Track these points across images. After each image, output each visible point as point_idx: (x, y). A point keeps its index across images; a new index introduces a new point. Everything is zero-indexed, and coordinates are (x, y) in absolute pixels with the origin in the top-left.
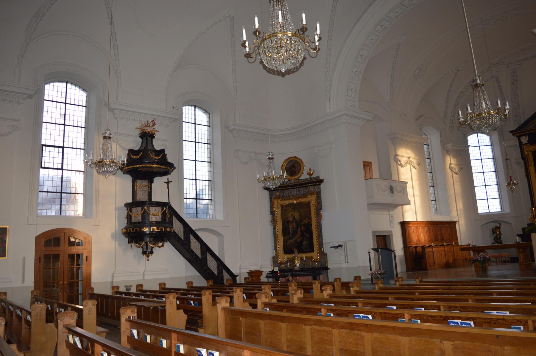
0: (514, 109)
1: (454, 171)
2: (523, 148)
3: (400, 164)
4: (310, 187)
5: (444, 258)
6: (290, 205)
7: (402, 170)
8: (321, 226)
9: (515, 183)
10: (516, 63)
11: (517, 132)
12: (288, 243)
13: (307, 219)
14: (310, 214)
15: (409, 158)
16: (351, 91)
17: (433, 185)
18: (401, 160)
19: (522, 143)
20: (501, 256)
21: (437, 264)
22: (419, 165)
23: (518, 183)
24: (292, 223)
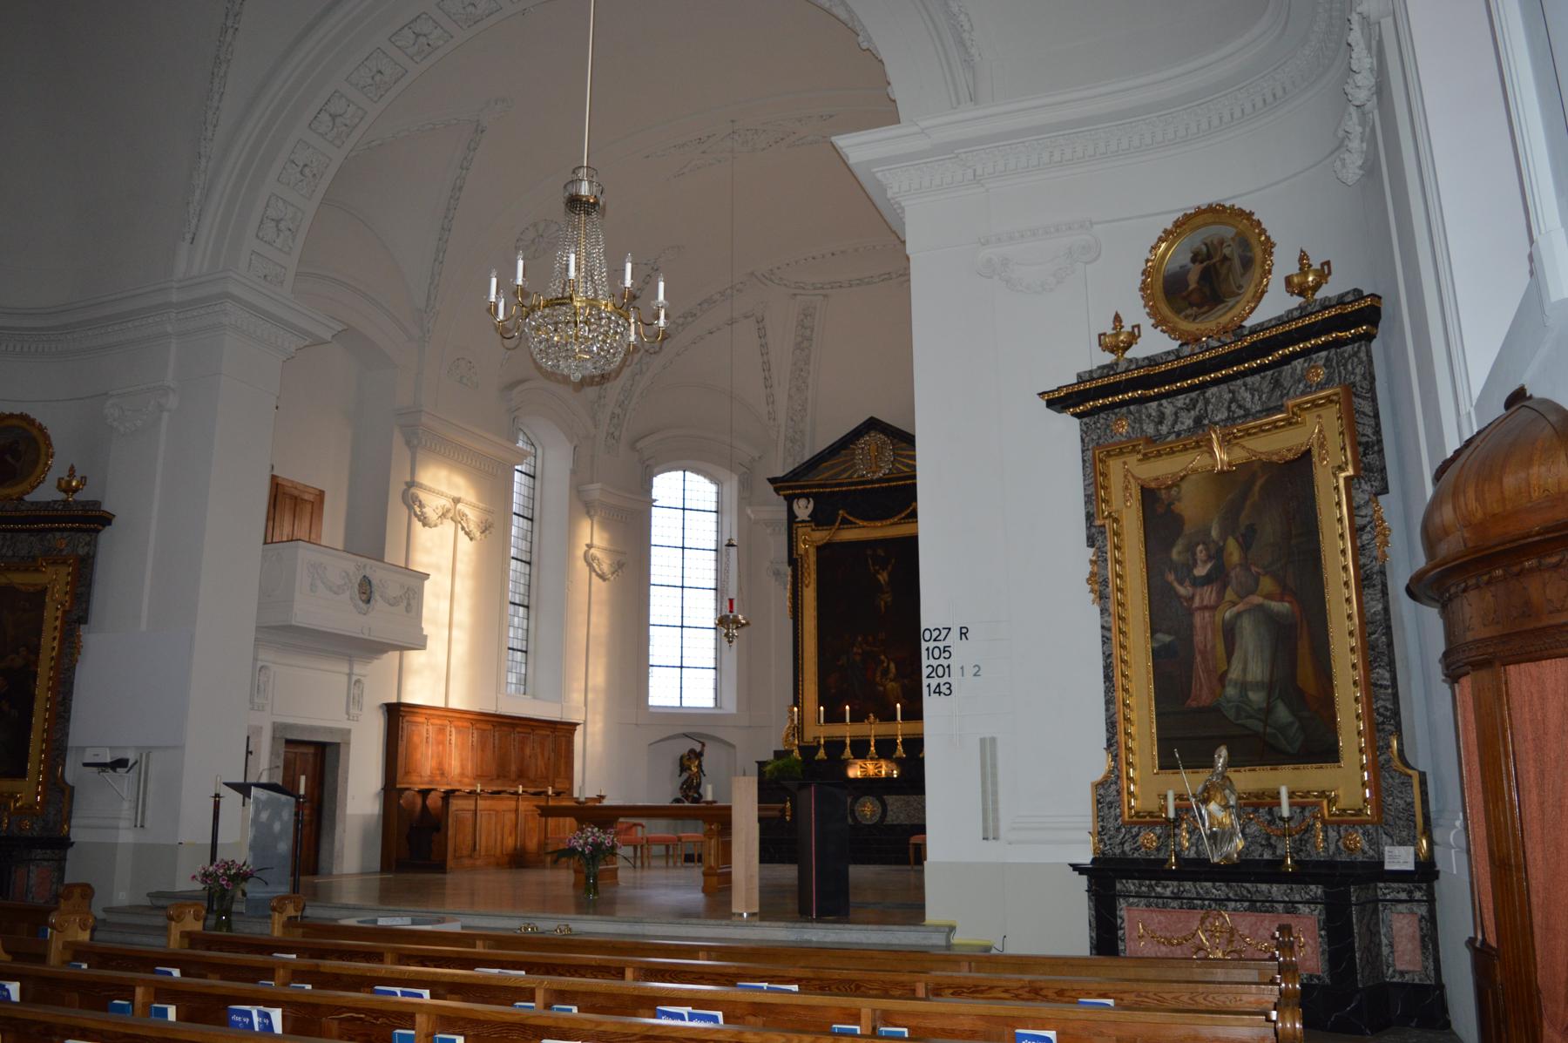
0: (792, 420)
1: (596, 567)
2: (796, 533)
3: (419, 513)
4: (58, 535)
5: (511, 835)
7: (422, 534)
8: (72, 684)
9: (739, 622)
10: (815, 289)
11: (787, 484)
14: (39, 632)
15: (457, 501)
16: (277, 226)
17: (526, 604)
18: (423, 502)
19: (797, 517)
20: (680, 839)
21: (483, 853)
22: (486, 529)
23: (748, 624)
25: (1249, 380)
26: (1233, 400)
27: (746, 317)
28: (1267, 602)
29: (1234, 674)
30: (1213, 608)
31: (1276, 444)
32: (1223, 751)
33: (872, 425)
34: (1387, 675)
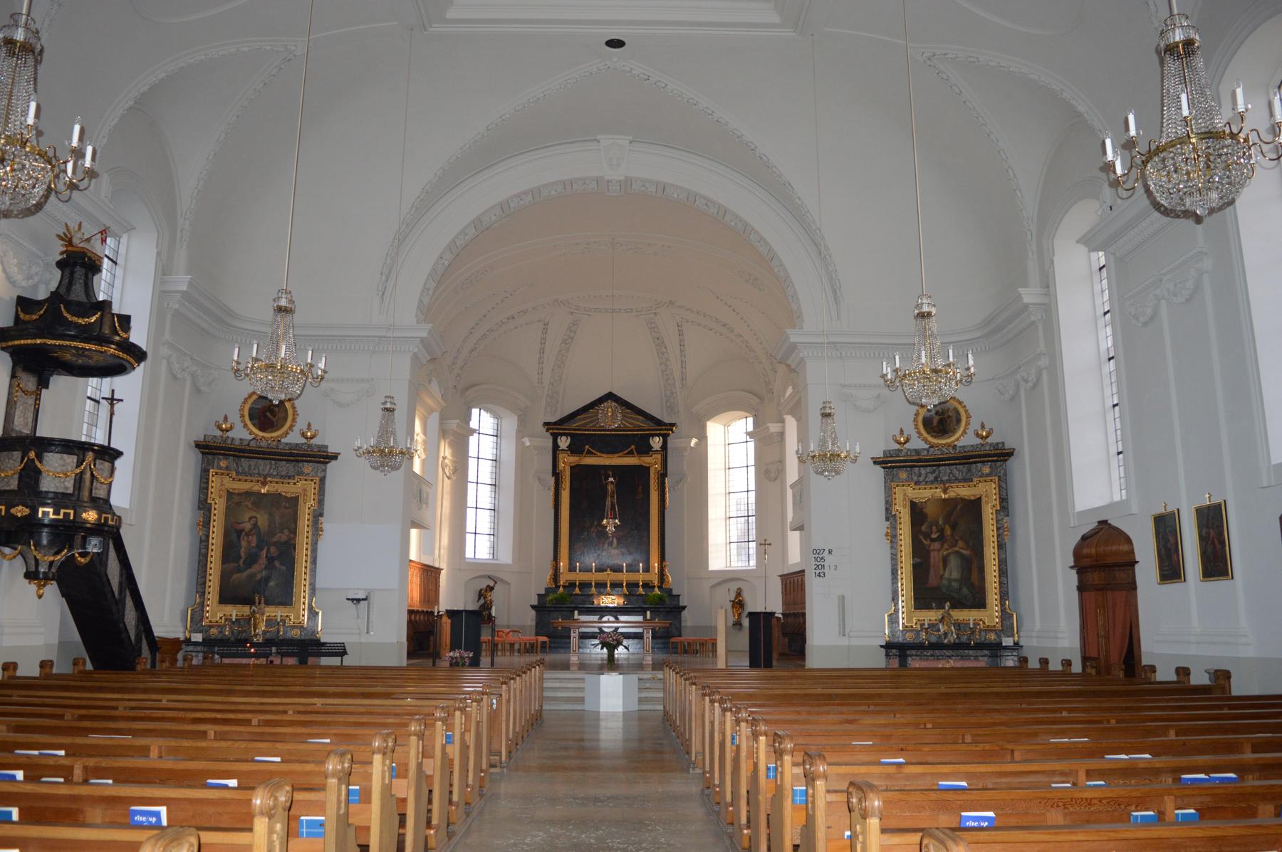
4: (305, 464)
6: (248, 494)
12: (232, 579)
13: (285, 531)
24: (248, 534)
25: (958, 466)
26: (951, 473)
27: (539, 321)
28: (961, 550)
29: (947, 575)
30: (939, 550)
31: (965, 492)
32: (948, 604)
33: (610, 396)
34: (1006, 580)
